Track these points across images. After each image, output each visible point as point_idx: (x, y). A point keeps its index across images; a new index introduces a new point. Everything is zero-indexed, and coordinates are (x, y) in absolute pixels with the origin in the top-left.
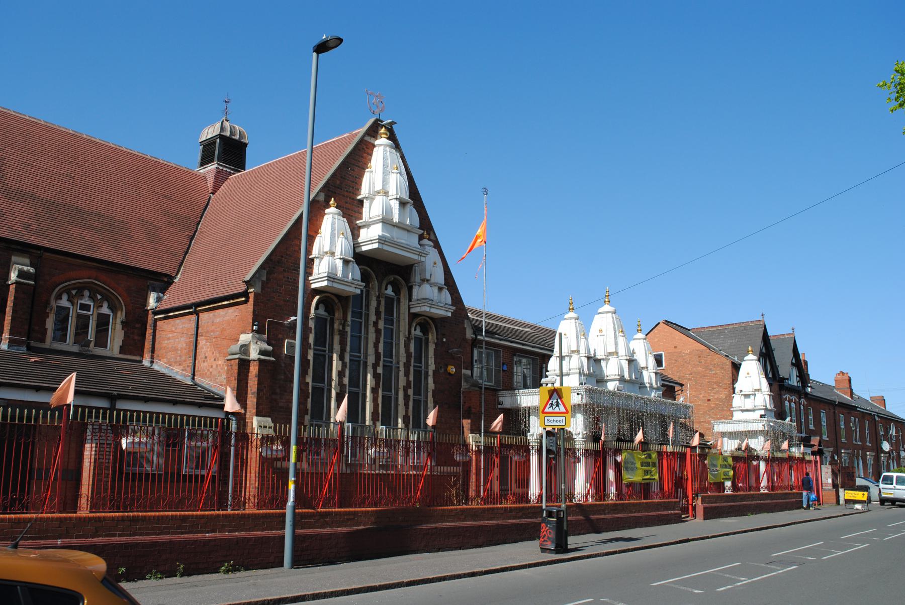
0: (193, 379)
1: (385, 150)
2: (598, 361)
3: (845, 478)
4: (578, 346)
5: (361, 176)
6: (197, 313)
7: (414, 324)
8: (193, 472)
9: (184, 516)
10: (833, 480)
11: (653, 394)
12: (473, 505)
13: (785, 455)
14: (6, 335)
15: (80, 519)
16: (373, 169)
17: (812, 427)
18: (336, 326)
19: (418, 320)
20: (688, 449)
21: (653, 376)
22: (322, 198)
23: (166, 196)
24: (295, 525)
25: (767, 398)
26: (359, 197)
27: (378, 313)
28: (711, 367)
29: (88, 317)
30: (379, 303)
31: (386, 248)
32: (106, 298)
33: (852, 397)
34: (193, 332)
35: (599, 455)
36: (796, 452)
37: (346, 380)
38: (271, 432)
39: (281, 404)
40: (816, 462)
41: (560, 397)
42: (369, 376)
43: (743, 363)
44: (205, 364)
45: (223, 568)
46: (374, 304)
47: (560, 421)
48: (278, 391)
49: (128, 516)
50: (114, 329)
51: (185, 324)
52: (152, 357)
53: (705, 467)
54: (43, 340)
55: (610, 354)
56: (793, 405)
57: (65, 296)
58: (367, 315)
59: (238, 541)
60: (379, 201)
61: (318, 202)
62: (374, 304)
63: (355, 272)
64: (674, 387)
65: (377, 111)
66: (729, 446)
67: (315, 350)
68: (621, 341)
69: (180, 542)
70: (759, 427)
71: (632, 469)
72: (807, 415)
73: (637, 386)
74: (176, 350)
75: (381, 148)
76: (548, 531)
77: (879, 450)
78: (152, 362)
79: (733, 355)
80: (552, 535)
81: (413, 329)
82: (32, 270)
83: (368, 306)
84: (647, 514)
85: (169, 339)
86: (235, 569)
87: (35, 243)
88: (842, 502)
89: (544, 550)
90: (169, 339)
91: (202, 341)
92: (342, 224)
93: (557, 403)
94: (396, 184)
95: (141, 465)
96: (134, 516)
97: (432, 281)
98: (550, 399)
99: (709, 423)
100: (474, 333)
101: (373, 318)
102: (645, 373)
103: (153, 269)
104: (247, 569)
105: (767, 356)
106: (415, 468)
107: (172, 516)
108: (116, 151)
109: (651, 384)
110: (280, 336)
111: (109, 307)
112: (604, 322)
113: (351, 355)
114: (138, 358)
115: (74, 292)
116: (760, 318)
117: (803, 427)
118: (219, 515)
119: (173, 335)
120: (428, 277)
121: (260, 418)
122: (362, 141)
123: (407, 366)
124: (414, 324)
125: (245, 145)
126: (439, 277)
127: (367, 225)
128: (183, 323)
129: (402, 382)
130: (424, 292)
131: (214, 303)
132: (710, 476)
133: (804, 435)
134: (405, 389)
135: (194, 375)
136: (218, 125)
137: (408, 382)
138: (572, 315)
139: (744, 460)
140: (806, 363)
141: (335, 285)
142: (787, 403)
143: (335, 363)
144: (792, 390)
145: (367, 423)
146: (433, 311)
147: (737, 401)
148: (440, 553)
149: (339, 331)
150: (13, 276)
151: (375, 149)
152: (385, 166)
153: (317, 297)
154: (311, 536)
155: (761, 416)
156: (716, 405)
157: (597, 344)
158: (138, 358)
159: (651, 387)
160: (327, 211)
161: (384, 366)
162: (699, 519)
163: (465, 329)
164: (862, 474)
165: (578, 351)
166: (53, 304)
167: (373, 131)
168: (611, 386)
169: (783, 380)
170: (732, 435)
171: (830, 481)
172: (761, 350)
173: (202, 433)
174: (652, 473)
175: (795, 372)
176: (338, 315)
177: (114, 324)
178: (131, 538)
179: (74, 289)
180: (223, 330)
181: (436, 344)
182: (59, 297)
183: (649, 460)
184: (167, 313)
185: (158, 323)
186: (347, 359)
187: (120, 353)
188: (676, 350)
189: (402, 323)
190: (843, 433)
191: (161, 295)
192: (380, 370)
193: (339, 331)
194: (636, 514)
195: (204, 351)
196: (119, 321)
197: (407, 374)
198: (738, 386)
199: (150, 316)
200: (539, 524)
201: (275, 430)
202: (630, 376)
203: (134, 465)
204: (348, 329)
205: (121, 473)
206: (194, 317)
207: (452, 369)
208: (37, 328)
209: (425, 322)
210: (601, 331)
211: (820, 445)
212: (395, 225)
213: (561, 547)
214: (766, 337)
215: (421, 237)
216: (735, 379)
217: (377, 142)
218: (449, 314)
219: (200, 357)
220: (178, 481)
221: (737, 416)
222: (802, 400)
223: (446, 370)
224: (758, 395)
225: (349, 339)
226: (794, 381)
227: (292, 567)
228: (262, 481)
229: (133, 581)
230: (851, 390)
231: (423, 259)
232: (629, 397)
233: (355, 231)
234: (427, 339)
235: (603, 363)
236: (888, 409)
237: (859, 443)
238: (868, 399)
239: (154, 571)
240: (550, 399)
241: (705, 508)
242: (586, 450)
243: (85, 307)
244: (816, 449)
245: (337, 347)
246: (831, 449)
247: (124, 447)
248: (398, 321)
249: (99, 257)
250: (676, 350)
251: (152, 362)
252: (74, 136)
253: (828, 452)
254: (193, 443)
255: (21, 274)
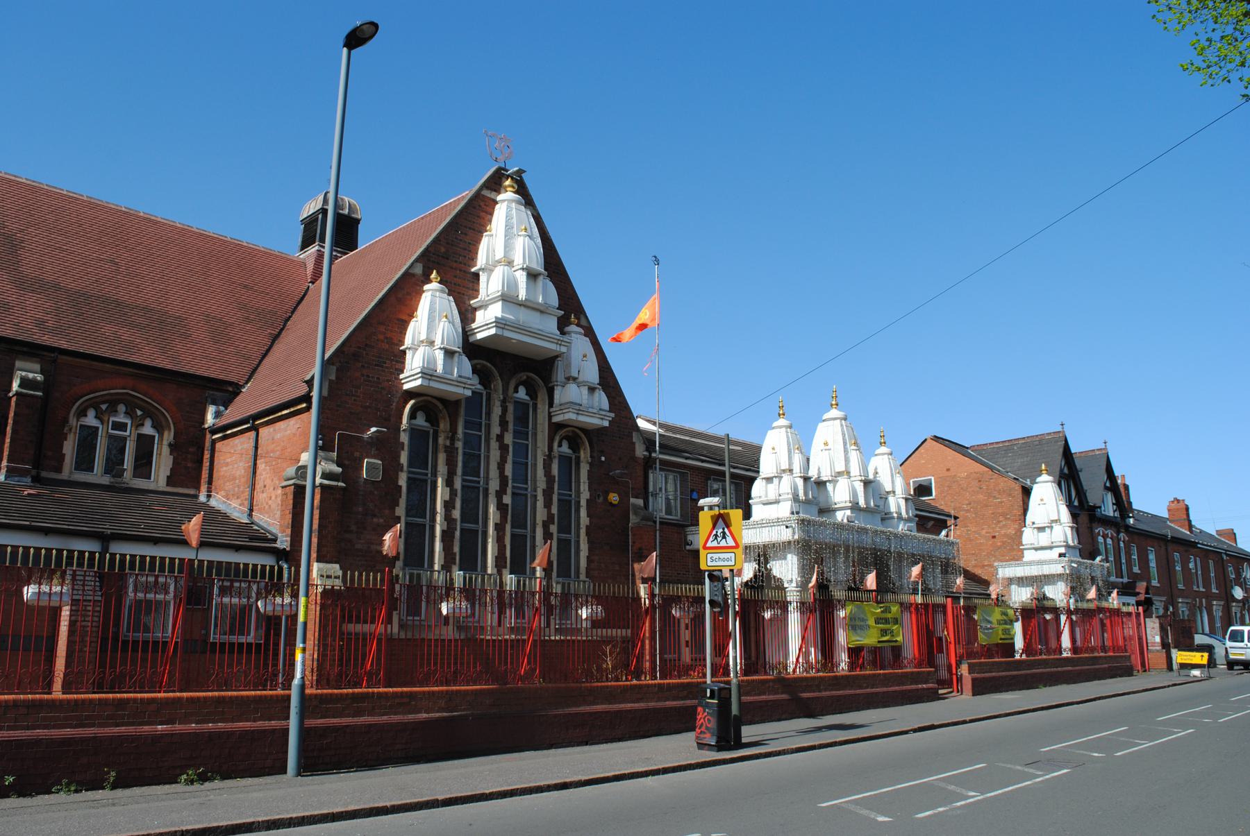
0: (250, 515)
1: (508, 207)
2: (821, 484)
3: (1180, 635)
4: (790, 463)
5: (478, 241)
6: (255, 429)
7: (557, 438)
8: (225, 638)
9: (121, 700)
10: (1162, 638)
11: (901, 527)
12: (646, 680)
13: (1092, 606)
14: (4, 463)
15: (53, 701)
16: (493, 232)
17: (1136, 570)
18: (441, 441)
19: (563, 432)
20: (949, 600)
21: (902, 503)
22: (418, 270)
23: (245, 286)
24: (302, 716)
25: (1069, 531)
26: (473, 270)
27: (503, 424)
28: (996, 494)
29: (124, 439)
30: (505, 410)
31: (507, 334)
32: (148, 414)
33: (1191, 532)
34: (252, 452)
35: (821, 608)
36: (1114, 601)
37: (456, 514)
38: (338, 584)
39: (358, 546)
40: (1138, 615)
41: (728, 525)
42: (492, 509)
43: (1035, 486)
44: (265, 495)
45: (185, 776)
46: (497, 411)
47: (728, 560)
48: (354, 528)
49: (24, 701)
50: (159, 454)
51: (244, 443)
52: (209, 490)
53: (973, 624)
54: (59, 469)
55: (840, 474)
56: (1109, 541)
57: (91, 413)
58: (488, 426)
59: (212, 737)
60: (499, 272)
61: (413, 275)
62: (497, 411)
63: (463, 367)
64: (945, 521)
65: (500, 157)
66: (1021, 596)
67: (409, 472)
68: (854, 456)
69: (112, 739)
70: (1057, 569)
71: (861, 628)
72: (1128, 555)
73: (878, 517)
74: (234, 479)
75: (506, 205)
76: (706, 718)
77: (1230, 598)
78: (209, 496)
79: (1024, 478)
80: (713, 724)
81: (556, 445)
82: (39, 377)
83: (489, 414)
84: (885, 689)
85: (227, 464)
86: (203, 778)
87: (48, 343)
88: (1175, 667)
89: (701, 746)
90: (227, 464)
91: (261, 465)
92: (447, 304)
93: (724, 533)
94: (525, 250)
95: (147, 630)
96: (33, 700)
97: (580, 379)
98: (714, 527)
99: (991, 566)
100: (647, 450)
101: (496, 430)
102: (891, 499)
103: (212, 376)
104: (225, 777)
105: (1070, 476)
106: (512, 630)
107: (100, 700)
108: (184, 232)
109: (899, 514)
110: (357, 454)
111: (154, 426)
112: (829, 434)
113: (464, 480)
114: (192, 492)
115: (104, 407)
116: (1059, 429)
117: (1124, 567)
118: (180, 699)
119: (231, 457)
120: (575, 374)
121: (322, 565)
122: (477, 196)
123: (548, 494)
124: (557, 438)
125: (358, 221)
126: (591, 373)
127: (484, 306)
128: (242, 443)
129: (541, 514)
130: (568, 394)
131: (273, 414)
132: (980, 636)
133: (1125, 580)
134: (546, 526)
135: (251, 510)
136: (321, 198)
137: (550, 518)
138: (782, 422)
139: (1037, 615)
140: (1126, 487)
141: (433, 384)
142: (1101, 539)
143: (439, 490)
144: (1106, 522)
145: (489, 571)
146: (581, 418)
147: (1029, 536)
148: (552, 751)
149: (446, 447)
150: (15, 386)
151: (497, 207)
152: (508, 227)
153: (412, 402)
154: (336, 729)
155: (1060, 555)
156: (1004, 543)
157: (816, 459)
158: (192, 492)
159: (900, 518)
160: (426, 287)
161: (513, 494)
162: (967, 696)
163: (634, 444)
164: (1207, 630)
165: (791, 471)
166: (73, 421)
167: (495, 182)
168: (841, 516)
169: (1095, 508)
170: (1022, 581)
171: (1158, 639)
172: (1061, 470)
173: (156, 582)
174: (905, 630)
175: (1109, 498)
176: (444, 425)
177: (160, 449)
178: (29, 733)
179: (104, 403)
180: (284, 449)
181: (591, 464)
182: (82, 413)
183: (889, 616)
184: (224, 431)
185: (218, 445)
186: (458, 484)
187: (168, 485)
188: (948, 474)
189: (539, 437)
190: (1180, 577)
191: (222, 408)
192: (507, 499)
193: (446, 447)
194: (869, 690)
195: (263, 475)
196: (165, 442)
197: (548, 505)
198: (1030, 518)
199: (208, 436)
200: (694, 708)
201: (344, 581)
202: (867, 501)
203: (136, 630)
204: (459, 445)
205: (116, 639)
206: (253, 434)
207: (614, 498)
208: (50, 453)
209: (575, 435)
210: (826, 444)
211: (1147, 593)
212: (521, 304)
213: (728, 738)
214: (1067, 453)
215: (563, 324)
216: (1025, 510)
217: (499, 198)
218: (606, 424)
219: (259, 486)
220: (115, 650)
221: (1029, 556)
222: (1122, 535)
223: (606, 499)
224: (1057, 528)
225: (460, 458)
226: (1109, 510)
227: (299, 774)
228: (324, 650)
229: (32, 796)
230: (1190, 521)
231: (564, 349)
232: (865, 531)
233: (467, 315)
234: (578, 458)
235: (829, 487)
236: (1240, 545)
237: (1202, 589)
238: (1214, 533)
239: (65, 781)
240: (714, 527)
241: (974, 680)
242: (802, 603)
243: (121, 426)
244: (1142, 597)
245: (442, 468)
246: (1164, 599)
247: (445, 612)
248: (535, 434)
249: (137, 360)
250: (948, 474)
251: (209, 496)
252: (128, 215)
253: (1159, 604)
254: (226, 600)
255: (25, 383)
